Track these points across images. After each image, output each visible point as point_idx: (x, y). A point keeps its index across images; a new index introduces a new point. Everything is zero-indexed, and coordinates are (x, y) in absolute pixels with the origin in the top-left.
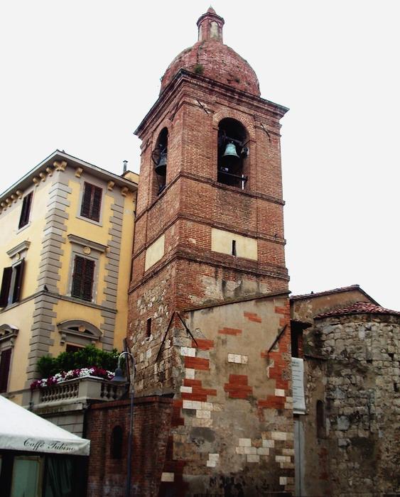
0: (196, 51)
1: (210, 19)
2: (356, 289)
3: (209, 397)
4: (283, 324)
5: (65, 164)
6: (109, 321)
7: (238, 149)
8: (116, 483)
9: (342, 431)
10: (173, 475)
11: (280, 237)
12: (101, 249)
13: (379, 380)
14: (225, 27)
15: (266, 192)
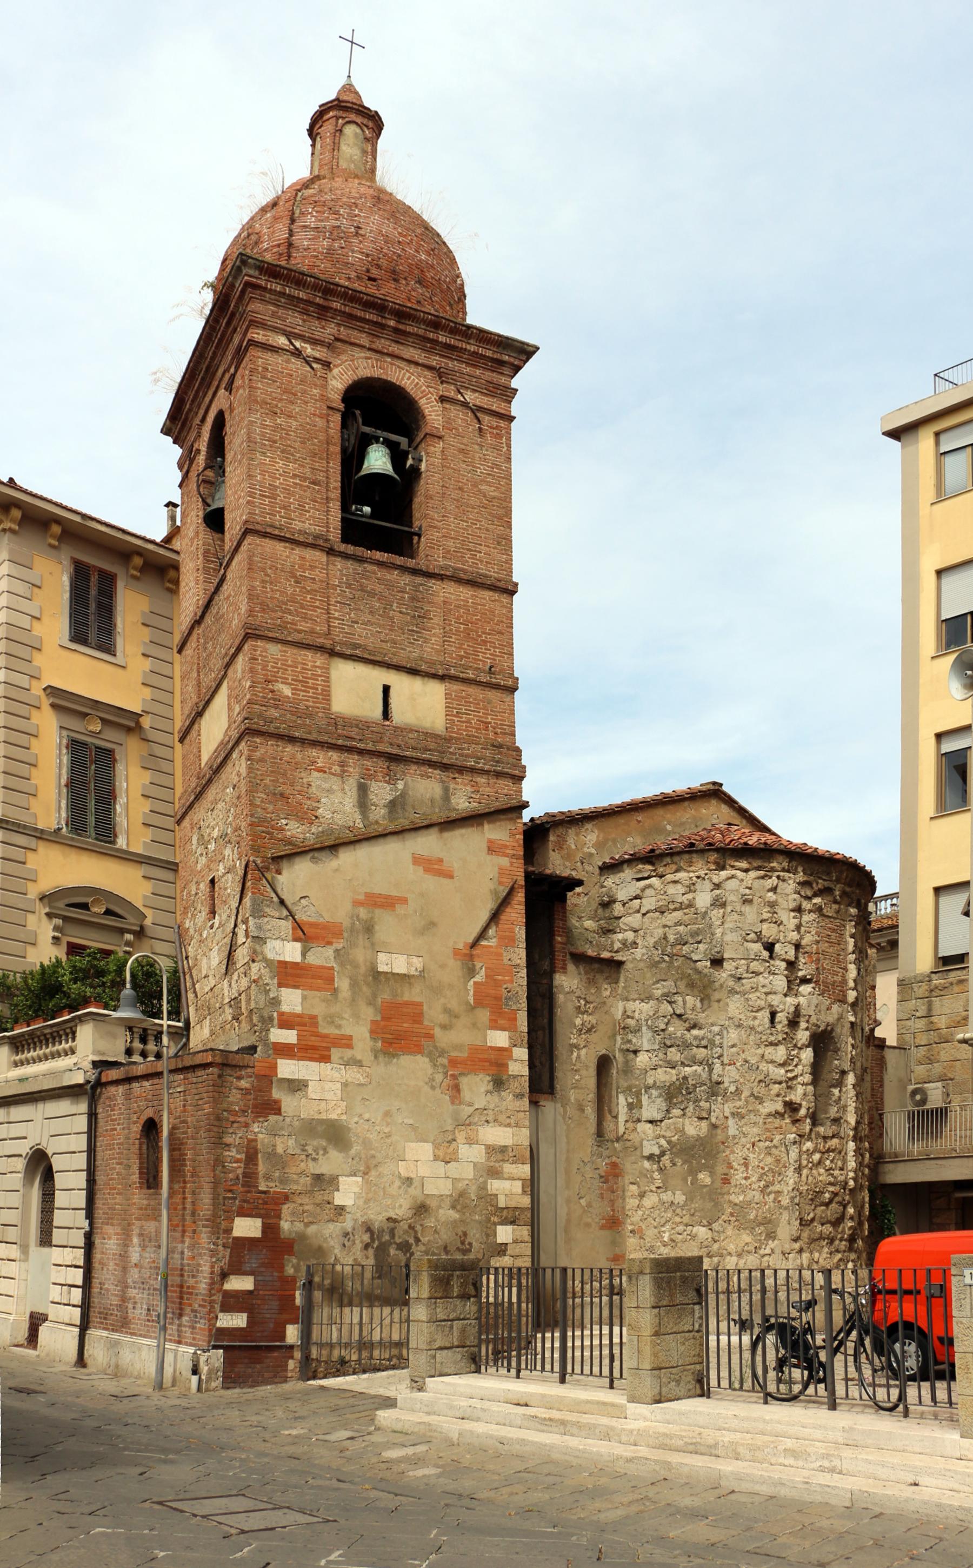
0: (287, 206)
1: (346, 118)
2: (715, 793)
3: (335, 1053)
5: (17, 514)
6: (164, 889)
7: (397, 457)
8: (150, 1241)
9: (651, 1122)
10: (258, 1222)
12: (127, 723)
13: (735, 1006)
14: (383, 142)
15: (468, 565)
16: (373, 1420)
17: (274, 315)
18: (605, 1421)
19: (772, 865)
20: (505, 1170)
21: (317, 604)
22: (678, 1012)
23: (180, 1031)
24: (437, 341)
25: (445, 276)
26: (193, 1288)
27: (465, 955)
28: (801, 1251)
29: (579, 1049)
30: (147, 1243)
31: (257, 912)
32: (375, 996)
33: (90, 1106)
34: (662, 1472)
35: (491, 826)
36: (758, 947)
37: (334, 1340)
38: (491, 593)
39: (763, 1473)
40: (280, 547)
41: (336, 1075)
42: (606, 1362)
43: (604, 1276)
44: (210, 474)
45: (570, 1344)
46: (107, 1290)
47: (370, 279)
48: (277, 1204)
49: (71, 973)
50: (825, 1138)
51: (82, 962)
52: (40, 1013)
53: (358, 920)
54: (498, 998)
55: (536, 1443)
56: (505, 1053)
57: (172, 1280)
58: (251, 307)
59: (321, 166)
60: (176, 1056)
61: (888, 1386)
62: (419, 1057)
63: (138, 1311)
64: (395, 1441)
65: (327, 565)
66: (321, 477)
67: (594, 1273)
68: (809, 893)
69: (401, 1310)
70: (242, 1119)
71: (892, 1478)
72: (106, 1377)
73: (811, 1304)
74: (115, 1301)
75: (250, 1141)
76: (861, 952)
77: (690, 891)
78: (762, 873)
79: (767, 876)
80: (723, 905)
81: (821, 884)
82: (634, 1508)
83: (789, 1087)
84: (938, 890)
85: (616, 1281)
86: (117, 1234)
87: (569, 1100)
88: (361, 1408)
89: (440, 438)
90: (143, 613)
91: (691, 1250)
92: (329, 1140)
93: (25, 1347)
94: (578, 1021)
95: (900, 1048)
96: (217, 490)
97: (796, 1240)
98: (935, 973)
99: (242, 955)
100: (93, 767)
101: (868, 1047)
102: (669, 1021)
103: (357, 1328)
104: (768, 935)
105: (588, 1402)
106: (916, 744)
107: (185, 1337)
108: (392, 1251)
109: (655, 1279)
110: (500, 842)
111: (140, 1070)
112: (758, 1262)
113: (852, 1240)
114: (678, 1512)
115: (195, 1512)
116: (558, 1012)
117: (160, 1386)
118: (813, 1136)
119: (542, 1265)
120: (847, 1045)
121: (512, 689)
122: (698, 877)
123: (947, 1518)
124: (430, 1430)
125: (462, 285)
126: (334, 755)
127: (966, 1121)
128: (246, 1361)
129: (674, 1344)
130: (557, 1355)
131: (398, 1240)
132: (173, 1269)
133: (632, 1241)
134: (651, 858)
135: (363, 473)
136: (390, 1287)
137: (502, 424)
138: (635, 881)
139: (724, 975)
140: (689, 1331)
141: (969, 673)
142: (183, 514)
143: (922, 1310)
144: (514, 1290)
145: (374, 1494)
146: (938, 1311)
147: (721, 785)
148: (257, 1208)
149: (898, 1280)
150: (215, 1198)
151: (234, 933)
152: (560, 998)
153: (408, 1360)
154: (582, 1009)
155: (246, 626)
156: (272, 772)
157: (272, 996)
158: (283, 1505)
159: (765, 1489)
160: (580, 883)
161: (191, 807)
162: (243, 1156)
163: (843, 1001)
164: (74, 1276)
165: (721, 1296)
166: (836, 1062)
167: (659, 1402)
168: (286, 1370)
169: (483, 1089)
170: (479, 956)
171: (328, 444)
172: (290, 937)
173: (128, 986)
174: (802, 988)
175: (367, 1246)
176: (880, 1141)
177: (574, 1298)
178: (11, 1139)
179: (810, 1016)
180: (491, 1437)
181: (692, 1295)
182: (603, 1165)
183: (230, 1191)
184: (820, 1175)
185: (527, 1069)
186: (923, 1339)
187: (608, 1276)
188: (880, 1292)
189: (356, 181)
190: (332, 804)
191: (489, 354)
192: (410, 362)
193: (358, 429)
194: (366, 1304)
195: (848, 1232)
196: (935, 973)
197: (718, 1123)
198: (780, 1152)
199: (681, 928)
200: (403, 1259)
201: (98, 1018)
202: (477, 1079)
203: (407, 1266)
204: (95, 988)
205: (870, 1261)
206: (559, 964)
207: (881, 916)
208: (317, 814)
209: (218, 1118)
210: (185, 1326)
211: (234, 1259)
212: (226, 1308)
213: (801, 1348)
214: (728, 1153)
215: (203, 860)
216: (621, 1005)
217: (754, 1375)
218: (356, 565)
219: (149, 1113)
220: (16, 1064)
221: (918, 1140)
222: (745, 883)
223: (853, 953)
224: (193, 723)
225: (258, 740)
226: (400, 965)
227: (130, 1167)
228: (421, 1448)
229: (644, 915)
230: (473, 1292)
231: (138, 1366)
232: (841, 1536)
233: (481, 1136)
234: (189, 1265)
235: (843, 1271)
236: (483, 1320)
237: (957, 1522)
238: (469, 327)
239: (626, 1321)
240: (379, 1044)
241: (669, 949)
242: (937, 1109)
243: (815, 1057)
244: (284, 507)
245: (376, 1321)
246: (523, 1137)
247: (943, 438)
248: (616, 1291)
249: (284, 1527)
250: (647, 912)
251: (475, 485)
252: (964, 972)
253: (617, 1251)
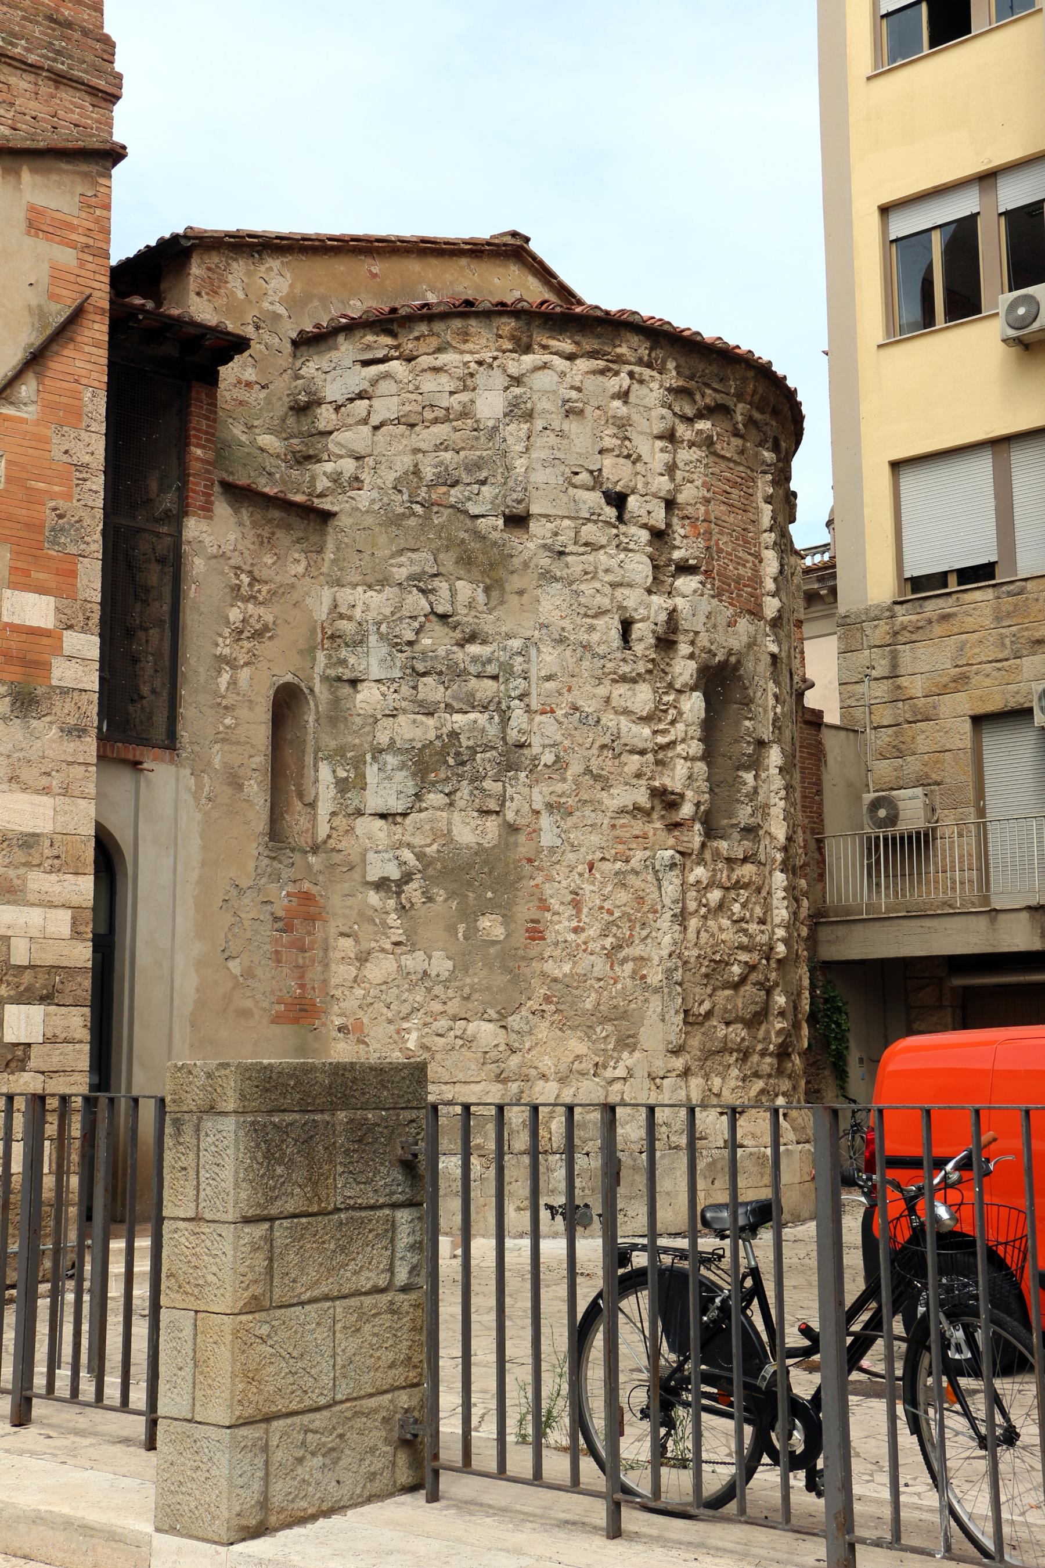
2: (513, 250)
4: (70, 300)
9: (383, 816)
13: (551, 604)
19: (618, 350)
22: (440, 610)
28: (686, 1073)
29: (234, 668)
35: (38, 179)
36: (595, 498)
56: (45, 641)
68: (689, 411)
77: (465, 388)
78: (601, 364)
79: (609, 370)
80: (529, 416)
81: (709, 397)
83: (658, 763)
84: (896, 466)
87: (209, 764)
95: (847, 730)
98: (901, 603)
102: (422, 626)
109: (256, 1130)
110: (58, 215)
113: (783, 1054)
116: (192, 592)
118: (708, 856)
122: (480, 363)
129: (321, 1334)
134: (389, 323)
138: (358, 367)
139: (531, 545)
147: (527, 240)
152: (197, 566)
154: (245, 590)
163: (755, 613)
166: (747, 723)
179: (697, 633)
181: (390, 1180)
182: (281, 897)
184: (721, 930)
185: (95, 677)
195: (776, 1040)
196: (901, 603)
197: (521, 822)
198: (645, 883)
199: (448, 456)
206: (196, 500)
213: (736, 1364)
214: (539, 880)
216: (327, 595)
217: (580, 1422)
222: (568, 379)
229: (376, 428)
241: (423, 493)
242: (918, 833)
243: (707, 710)
246: (80, 819)
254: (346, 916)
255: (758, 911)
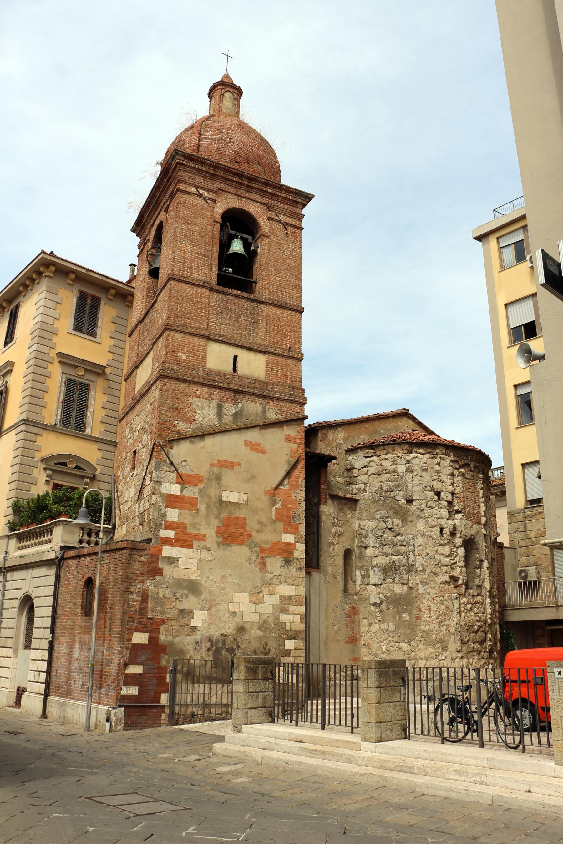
0: (198, 128)
1: (225, 90)
2: (405, 414)
3: (195, 544)
5: (53, 268)
6: (109, 455)
7: (247, 245)
9: (375, 585)
10: (147, 635)
11: (295, 350)
12: (98, 371)
13: (420, 525)
16: (211, 749)
17: (190, 177)
18: (348, 752)
20: (290, 609)
21: (203, 314)
22: (389, 527)
23: (109, 530)
24: (267, 192)
25: (271, 162)
26: (108, 672)
27: (271, 493)
28: (462, 658)
29: (334, 545)
30: (83, 647)
31: (158, 468)
32: (220, 514)
33: (57, 571)
34: (382, 782)
35: (287, 427)
36: (432, 494)
37: (189, 703)
38: (291, 312)
39: (441, 784)
40: (186, 286)
41: (195, 555)
42: (349, 718)
43: (348, 669)
44: (153, 251)
45: (327, 707)
46: (60, 673)
47: (236, 162)
48: (158, 625)
49: (53, 499)
50: (473, 596)
51: (59, 493)
52: (35, 521)
53: (213, 474)
54: (289, 517)
55: (307, 764)
56: (292, 546)
57: (97, 668)
58: (179, 174)
59: (214, 111)
60: (106, 543)
61: (513, 735)
62: (243, 547)
63: (76, 686)
64: (224, 762)
65: (209, 296)
66: (209, 254)
67: (342, 667)
68: (457, 466)
69: (228, 686)
70: (141, 578)
71: (516, 788)
72: (58, 724)
73: (468, 688)
74: (64, 680)
75: (144, 590)
76: (487, 497)
78: (432, 455)
80: (412, 472)
81: (463, 462)
82: (366, 803)
83: (452, 568)
84: (523, 465)
85: (355, 672)
86: (67, 642)
87: (328, 572)
88: (204, 742)
89: (267, 237)
90: (113, 317)
91: (399, 656)
92: (189, 591)
93: (14, 707)
94: (333, 530)
96: (156, 259)
97: (459, 652)
99: (147, 490)
100: (78, 393)
101: (494, 547)
102: (384, 531)
103: (202, 696)
104: (437, 488)
105: (338, 741)
106: (505, 390)
107: (103, 700)
108: (224, 653)
109: (378, 672)
111: (86, 551)
112: (438, 663)
113: (491, 652)
114: (391, 806)
115: (109, 803)
116: (322, 525)
117: (88, 729)
118: (467, 595)
119: (311, 662)
120: (483, 546)
121: (301, 359)
122: (398, 457)
123: (547, 812)
124: (245, 756)
125: (279, 166)
126: (206, 389)
127: (550, 588)
128: (137, 714)
129: (389, 709)
130: (319, 713)
131: (227, 647)
132: (97, 661)
133: (364, 650)
134: (373, 446)
135: (229, 252)
136: (222, 672)
137: (297, 231)
139: (414, 508)
140: (398, 702)
141: (526, 354)
142: (138, 269)
143: (532, 692)
144: (295, 676)
145: (212, 793)
146: (541, 692)
147: (408, 410)
148: (146, 627)
149: (517, 675)
150: (123, 622)
151: (144, 479)
152: (324, 518)
153: (232, 714)
155: (165, 324)
156: (172, 397)
157: (162, 512)
158: (160, 799)
159: (442, 794)
160: (335, 458)
161: (127, 413)
162: (140, 598)
163: (479, 523)
164: (42, 666)
165: (416, 682)
167: (380, 741)
168: (160, 720)
169: (279, 565)
170: (278, 494)
171: (213, 238)
172: (175, 482)
173: (84, 506)
174: (456, 516)
175: (209, 650)
176: (504, 598)
177: (330, 681)
178: (13, 589)
179: (462, 531)
180: (281, 760)
181: (400, 681)
182: (347, 608)
183: (132, 618)
184: (471, 616)
186: (533, 708)
187: (350, 669)
188: (508, 681)
189: (230, 118)
190: (203, 414)
191: (291, 198)
192: (254, 201)
193: (228, 231)
194: (207, 682)
195: (488, 648)
197: (413, 586)
199: (390, 483)
200: (229, 657)
201: (66, 523)
202: (276, 559)
203: (232, 661)
204: (65, 507)
205: (502, 664)
206: (323, 500)
207: (495, 478)
208: (195, 419)
209: (127, 578)
210: (103, 694)
211: (132, 656)
212: (126, 684)
214: (419, 603)
215: (131, 441)
216: (357, 522)
217: (436, 727)
218: (224, 296)
219: (89, 574)
220: (19, 549)
221: (525, 598)
222: (423, 460)
223: (483, 497)
224: (133, 371)
225: (166, 381)
226: (234, 497)
227: (76, 604)
228: (240, 766)
229: (370, 475)
230: (270, 677)
231: (76, 717)
232: (486, 821)
233: (277, 590)
234: (106, 659)
235: (486, 669)
236: (276, 692)
237: (553, 814)
238: (282, 185)
239: (361, 694)
240: (221, 539)
242: (534, 581)
244: (190, 268)
245: (213, 692)
246: (301, 591)
247: (500, 240)
248: (355, 678)
249: (161, 812)
250: (371, 474)
251: (284, 260)
252: (542, 508)
253: (356, 655)
254: (365, 613)
255: (482, 610)
